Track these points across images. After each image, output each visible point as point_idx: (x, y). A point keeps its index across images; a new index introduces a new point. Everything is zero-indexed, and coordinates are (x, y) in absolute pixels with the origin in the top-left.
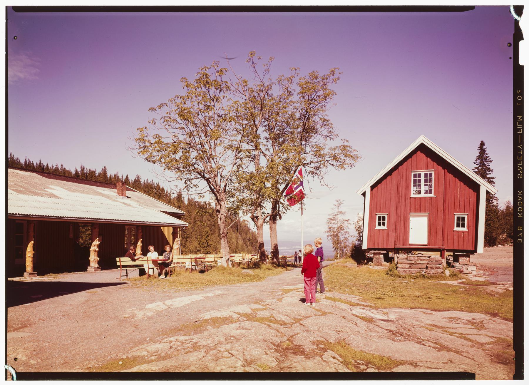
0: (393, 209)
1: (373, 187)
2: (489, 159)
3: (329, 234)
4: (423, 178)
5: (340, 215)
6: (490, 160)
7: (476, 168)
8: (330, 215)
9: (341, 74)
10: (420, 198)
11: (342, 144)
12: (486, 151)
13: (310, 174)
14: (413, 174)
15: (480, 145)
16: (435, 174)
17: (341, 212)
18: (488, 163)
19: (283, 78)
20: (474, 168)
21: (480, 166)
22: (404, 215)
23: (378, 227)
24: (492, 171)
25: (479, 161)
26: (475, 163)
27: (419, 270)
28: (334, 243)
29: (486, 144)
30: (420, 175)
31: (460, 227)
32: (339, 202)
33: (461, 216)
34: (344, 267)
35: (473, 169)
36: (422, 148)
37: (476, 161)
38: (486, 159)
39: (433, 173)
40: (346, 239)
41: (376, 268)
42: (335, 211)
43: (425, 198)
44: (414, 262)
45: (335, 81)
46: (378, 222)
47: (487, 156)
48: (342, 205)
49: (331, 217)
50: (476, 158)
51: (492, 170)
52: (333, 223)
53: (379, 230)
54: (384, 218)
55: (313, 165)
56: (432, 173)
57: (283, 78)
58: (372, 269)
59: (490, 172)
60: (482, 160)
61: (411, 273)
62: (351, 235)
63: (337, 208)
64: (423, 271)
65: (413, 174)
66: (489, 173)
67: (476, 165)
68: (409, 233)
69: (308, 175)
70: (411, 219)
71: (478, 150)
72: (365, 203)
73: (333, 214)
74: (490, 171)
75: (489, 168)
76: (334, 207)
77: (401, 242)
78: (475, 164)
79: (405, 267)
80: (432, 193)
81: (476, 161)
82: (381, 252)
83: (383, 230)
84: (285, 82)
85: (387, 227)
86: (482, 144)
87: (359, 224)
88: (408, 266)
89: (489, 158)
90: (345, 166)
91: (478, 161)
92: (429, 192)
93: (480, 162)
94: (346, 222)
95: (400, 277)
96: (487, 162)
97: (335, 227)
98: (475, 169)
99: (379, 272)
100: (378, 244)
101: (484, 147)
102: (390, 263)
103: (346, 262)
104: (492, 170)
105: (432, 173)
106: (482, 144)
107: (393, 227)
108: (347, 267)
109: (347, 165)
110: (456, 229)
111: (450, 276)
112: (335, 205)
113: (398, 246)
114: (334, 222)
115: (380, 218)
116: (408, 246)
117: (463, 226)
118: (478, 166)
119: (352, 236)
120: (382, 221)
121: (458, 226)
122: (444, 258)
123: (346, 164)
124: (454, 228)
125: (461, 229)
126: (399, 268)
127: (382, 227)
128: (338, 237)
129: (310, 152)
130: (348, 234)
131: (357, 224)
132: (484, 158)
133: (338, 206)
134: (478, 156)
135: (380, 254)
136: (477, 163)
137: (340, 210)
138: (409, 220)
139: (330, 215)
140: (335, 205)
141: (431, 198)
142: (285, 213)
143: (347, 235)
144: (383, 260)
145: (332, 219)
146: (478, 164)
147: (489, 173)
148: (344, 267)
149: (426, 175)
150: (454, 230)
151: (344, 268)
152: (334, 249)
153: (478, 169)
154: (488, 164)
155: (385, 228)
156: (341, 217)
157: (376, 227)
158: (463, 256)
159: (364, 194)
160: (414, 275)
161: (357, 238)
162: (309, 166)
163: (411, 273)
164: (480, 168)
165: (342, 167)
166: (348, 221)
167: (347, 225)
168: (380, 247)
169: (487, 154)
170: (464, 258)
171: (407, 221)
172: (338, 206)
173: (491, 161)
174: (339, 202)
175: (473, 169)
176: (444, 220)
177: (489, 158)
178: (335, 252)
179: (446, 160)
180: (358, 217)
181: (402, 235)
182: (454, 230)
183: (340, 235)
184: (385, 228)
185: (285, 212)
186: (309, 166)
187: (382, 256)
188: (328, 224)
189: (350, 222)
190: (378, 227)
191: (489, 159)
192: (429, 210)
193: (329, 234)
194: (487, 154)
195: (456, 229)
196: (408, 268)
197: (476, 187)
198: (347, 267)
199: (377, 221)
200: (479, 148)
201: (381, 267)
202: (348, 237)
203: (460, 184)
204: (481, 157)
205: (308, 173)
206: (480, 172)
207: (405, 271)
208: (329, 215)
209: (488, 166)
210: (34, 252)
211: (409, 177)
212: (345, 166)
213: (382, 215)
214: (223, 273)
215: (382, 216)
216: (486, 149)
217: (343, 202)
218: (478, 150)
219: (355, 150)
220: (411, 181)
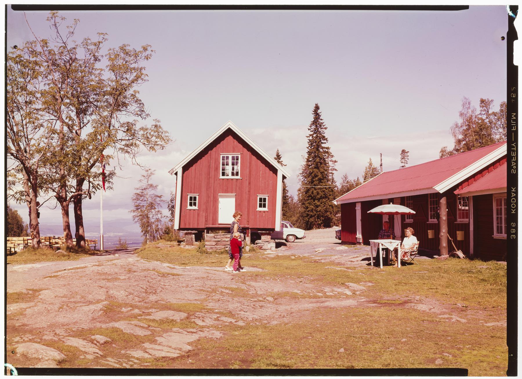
0: (204, 189)
1: (186, 168)
2: (324, 126)
3: (135, 214)
4: (230, 161)
5: (150, 189)
6: (325, 127)
7: (310, 135)
8: (137, 189)
9: (154, 52)
10: (228, 179)
11: (154, 124)
12: (320, 116)
13: (120, 151)
14: (221, 156)
15: (314, 108)
16: (241, 157)
17: (151, 186)
18: (323, 130)
19: (89, 41)
20: (309, 135)
21: (315, 133)
22: (214, 195)
23: (189, 207)
24: (326, 139)
25: (313, 127)
26: (309, 129)
27: (224, 246)
28: (143, 225)
29: (320, 108)
30: (228, 158)
31: (262, 207)
32: (149, 172)
33: (263, 197)
34: (156, 248)
35: (307, 137)
36: (229, 132)
37: (311, 127)
38: (321, 126)
39: (240, 156)
40: (158, 220)
41: (187, 247)
42: (144, 184)
43: (232, 179)
44: (219, 240)
45: (147, 58)
46: (196, 201)
47: (321, 121)
48: (152, 176)
49: (138, 192)
50: (310, 123)
51: (327, 139)
52: (141, 199)
53: (190, 210)
54: (195, 198)
55: (124, 143)
56: (238, 156)
57: (89, 41)
58: (183, 248)
59: (325, 141)
60: (316, 126)
61: (217, 249)
62: (163, 215)
63: (146, 180)
64: (227, 248)
65: (221, 156)
66: (324, 142)
67: (311, 131)
68: (218, 213)
69: (118, 152)
70: (221, 200)
71: (313, 114)
72: (176, 183)
73: (140, 188)
74: (324, 140)
75: (324, 137)
76: (143, 178)
77: (211, 222)
78: (309, 131)
79: (212, 244)
80: (238, 176)
81: (311, 127)
82: (193, 232)
83: (194, 210)
84: (92, 47)
85: (198, 207)
86: (317, 108)
87: (173, 203)
88: (214, 243)
89: (324, 124)
90: (156, 147)
91: (312, 127)
92: (236, 174)
93: (315, 128)
94: (158, 199)
95: (207, 253)
96: (322, 128)
97: (144, 205)
98: (309, 136)
99: (189, 251)
100: (189, 224)
101: (319, 111)
102: (199, 241)
103: (158, 243)
104: (327, 139)
105: (238, 156)
106: (317, 108)
107: (203, 207)
108: (159, 248)
109: (159, 147)
110: (259, 209)
111: (249, 251)
112: (144, 176)
113: (208, 226)
114: (143, 198)
115: (191, 198)
116: (217, 226)
117: (264, 206)
118: (312, 133)
119: (165, 216)
120: (193, 201)
121: (260, 206)
122: (249, 236)
123: (157, 145)
124: (257, 209)
125: (262, 209)
126: (207, 245)
127: (193, 207)
128: (148, 218)
129: (119, 127)
130: (161, 214)
131: (170, 203)
132: (318, 124)
133: (147, 177)
134: (312, 121)
135: (191, 234)
136: (311, 130)
137: (150, 183)
138: (218, 200)
139: (137, 189)
140: (144, 176)
141: (237, 180)
142: (95, 193)
143: (159, 216)
144: (194, 240)
145: (139, 195)
146: (312, 131)
147: (324, 142)
148: (156, 248)
149: (233, 158)
150: (257, 210)
151: (156, 249)
152: (142, 234)
153: (312, 137)
154: (323, 131)
155: (196, 208)
156: (150, 192)
157: (187, 208)
158: (264, 234)
159: (176, 174)
160: (219, 251)
161: (170, 218)
162: (120, 143)
163: (217, 249)
164: (315, 135)
165: (152, 148)
166: (160, 197)
167: (159, 202)
168: (191, 227)
169: (321, 120)
170: (266, 236)
171: (216, 202)
172: (147, 177)
173: (326, 128)
174: (149, 172)
175: (307, 137)
176: (249, 201)
177: (324, 124)
178: (144, 237)
179: (249, 145)
180: (171, 195)
181: (211, 215)
182: (257, 210)
183: (150, 216)
184: (196, 208)
185: (95, 191)
186: (120, 143)
187: (194, 235)
188: (134, 201)
189: (163, 198)
190: (189, 207)
191: (324, 126)
192: (236, 192)
193: (135, 214)
194: (321, 120)
195: (259, 209)
196: (215, 245)
197: (275, 171)
198: (159, 248)
199: (189, 201)
200: (313, 111)
201: (192, 247)
202: (160, 218)
203: (262, 166)
204: (316, 123)
205: (117, 150)
206: (314, 140)
207: (211, 248)
208: (135, 189)
209: (323, 134)
210: (391, 203)
211: (218, 159)
212: (156, 147)
213: (193, 195)
214: (36, 254)
215: (193, 196)
216: (320, 114)
217: (154, 173)
218: (313, 114)
219: (166, 132)
220: (220, 163)
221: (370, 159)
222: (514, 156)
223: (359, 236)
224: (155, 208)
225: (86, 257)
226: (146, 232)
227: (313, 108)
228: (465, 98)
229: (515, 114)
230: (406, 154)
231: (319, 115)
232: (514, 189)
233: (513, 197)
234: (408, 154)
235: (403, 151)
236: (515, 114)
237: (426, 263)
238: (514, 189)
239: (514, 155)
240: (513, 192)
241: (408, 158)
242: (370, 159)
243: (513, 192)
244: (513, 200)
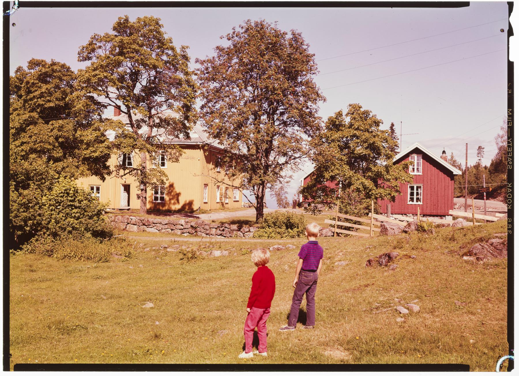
29: (395, 125)
86: (393, 125)
106: (393, 125)
221: (452, 154)
222: (510, 152)
223: (485, 198)
224: (284, 190)
225: (225, 218)
226: (280, 204)
227: (390, 125)
228: (350, 105)
229: (511, 110)
230: (482, 150)
231: (394, 131)
232: (510, 185)
233: (509, 193)
234: (484, 150)
235: (480, 148)
236: (511, 110)
237: (102, 317)
238: (510, 185)
239: (510, 151)
240: (509, 188)
241: (484, 153)
242: (452, 154)
243: (509, 188)
244: (509, 196)
